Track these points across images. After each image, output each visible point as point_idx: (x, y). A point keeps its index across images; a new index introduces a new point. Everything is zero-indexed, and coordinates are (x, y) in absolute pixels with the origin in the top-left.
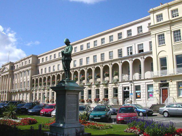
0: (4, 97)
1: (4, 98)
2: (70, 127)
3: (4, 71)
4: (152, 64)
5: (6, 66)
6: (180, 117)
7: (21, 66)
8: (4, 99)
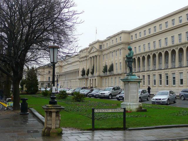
0: (94, 82)
1: (94, 84)
2: (131, 104)
3: (92, 51)
4: (140, 61)
5: (95, 46)
6: (103, 99)
7: (111, 44)
8: (94, 85)
